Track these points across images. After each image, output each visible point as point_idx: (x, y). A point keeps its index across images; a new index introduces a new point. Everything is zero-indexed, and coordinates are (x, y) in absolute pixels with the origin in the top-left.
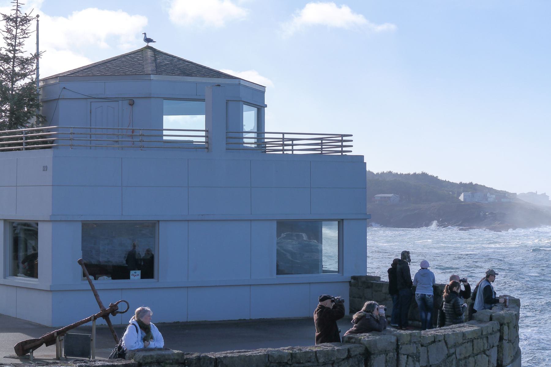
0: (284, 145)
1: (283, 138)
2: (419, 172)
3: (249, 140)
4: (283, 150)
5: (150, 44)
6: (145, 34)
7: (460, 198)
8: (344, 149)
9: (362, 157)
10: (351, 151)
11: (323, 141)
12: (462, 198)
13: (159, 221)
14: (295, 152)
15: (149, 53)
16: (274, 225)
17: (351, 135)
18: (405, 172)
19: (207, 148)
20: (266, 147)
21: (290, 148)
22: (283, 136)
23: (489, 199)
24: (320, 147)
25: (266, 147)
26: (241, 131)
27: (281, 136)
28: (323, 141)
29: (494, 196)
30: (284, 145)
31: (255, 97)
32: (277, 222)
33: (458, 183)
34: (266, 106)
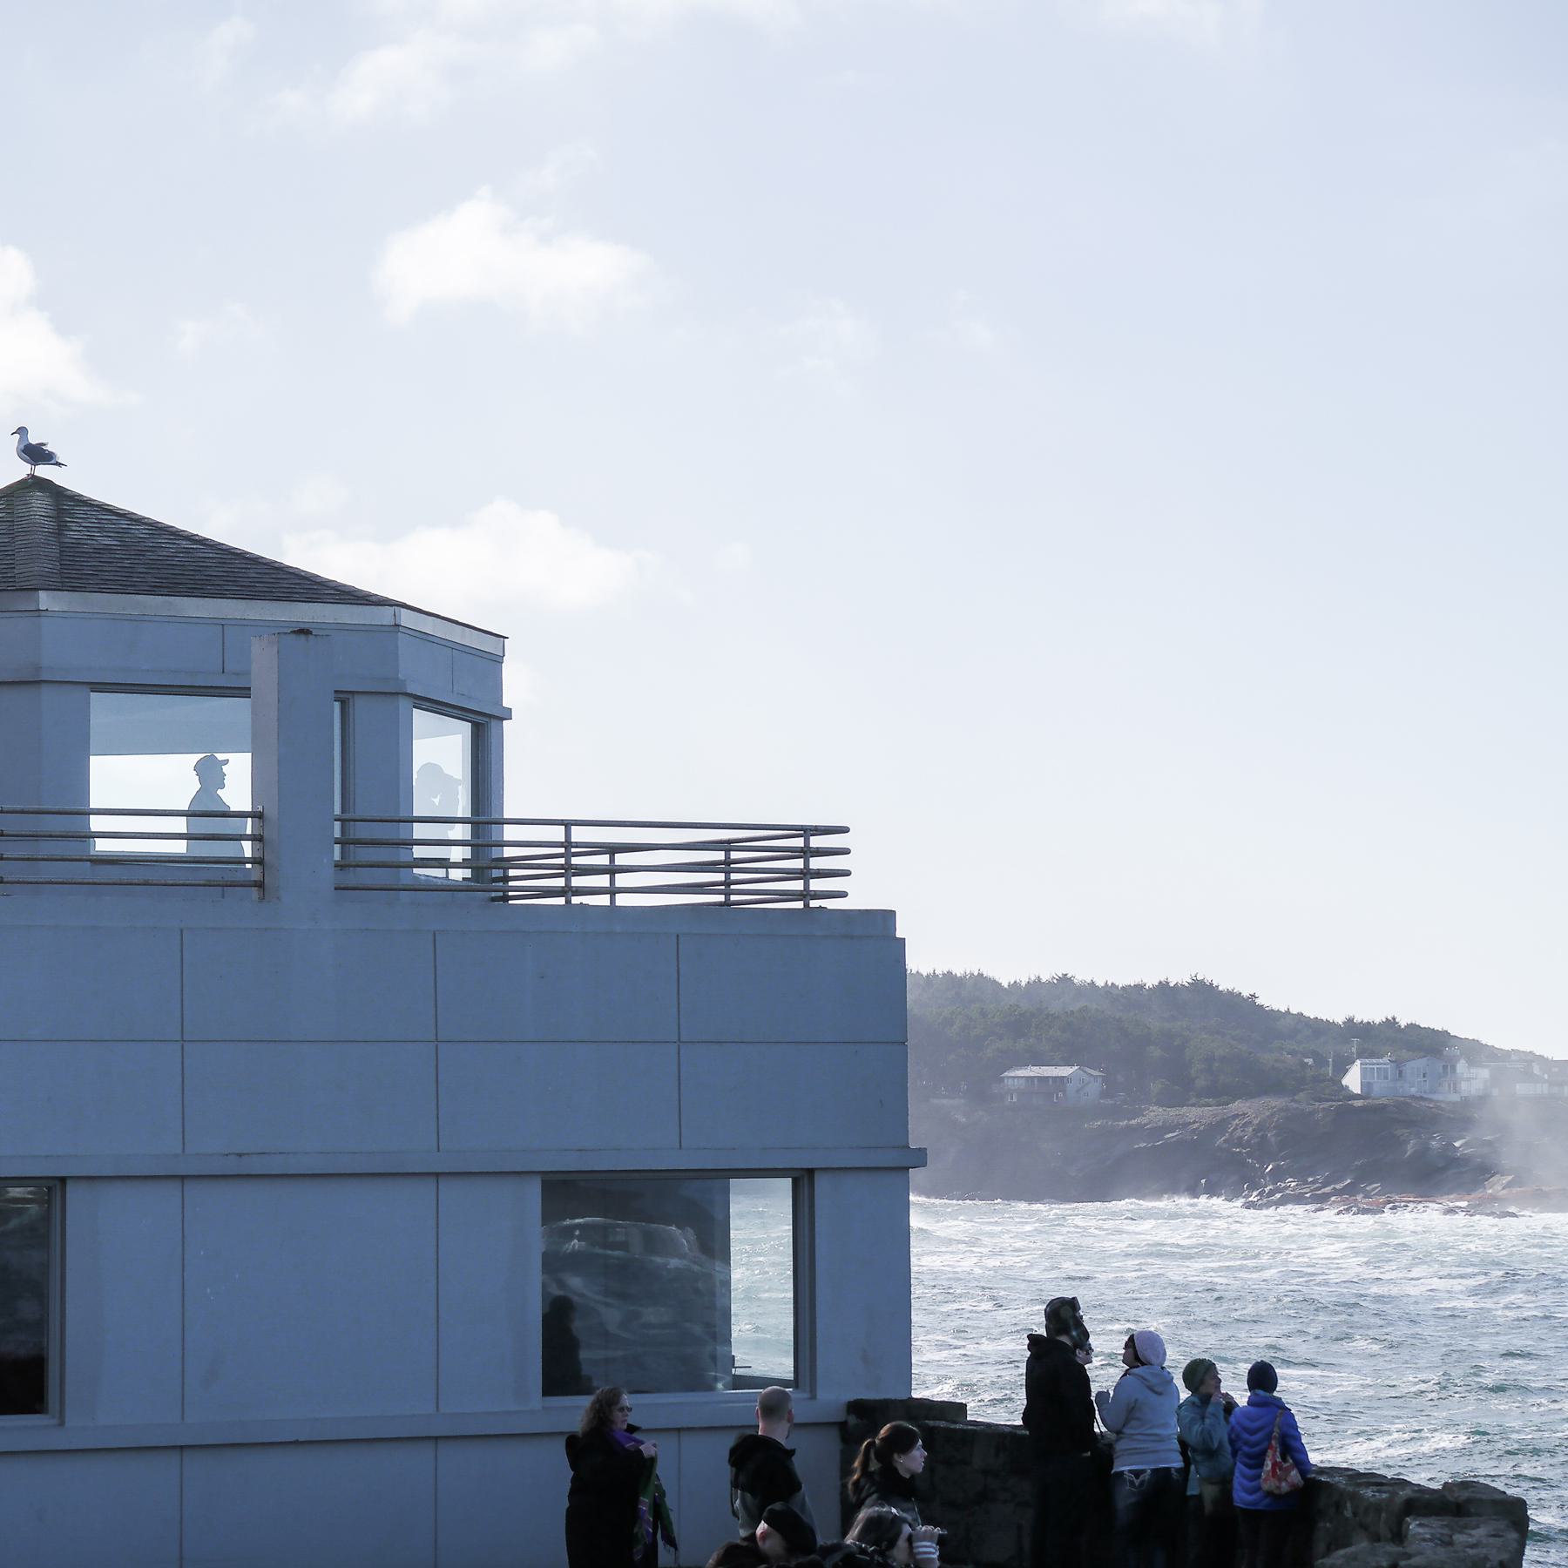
0: (569, 870)
1: (568, 844)
2: (1179, 976)
3: (444, 848)
4: (612, 891)
5: (43, 471)
6: (22, 431)
7: (1345, 1082)
8: (816, 885)
9: (888, 917)
10: (843, 895)
11: (734, 855)
12: (1353, 1080)
13: (63, 1180)
14: (622, 900)
15: (39, 504)
16: (533, 1192)
17: (845, 830)
18: (1123, 979)
19: (260, 885)
20: (506, 879)
21: (603, 881)
22: (568, 834)
23: (1463, 1086)
24: (721, 877)
25: (506, 879)
26: (403, 814)
27: (557, 834)
28: (734, 855)
29: (1484, 1073)
30: (569, 870)
31: (464, 677)
32: (543, 1182)
33: (1340, 1019)
34: (507, 714)
